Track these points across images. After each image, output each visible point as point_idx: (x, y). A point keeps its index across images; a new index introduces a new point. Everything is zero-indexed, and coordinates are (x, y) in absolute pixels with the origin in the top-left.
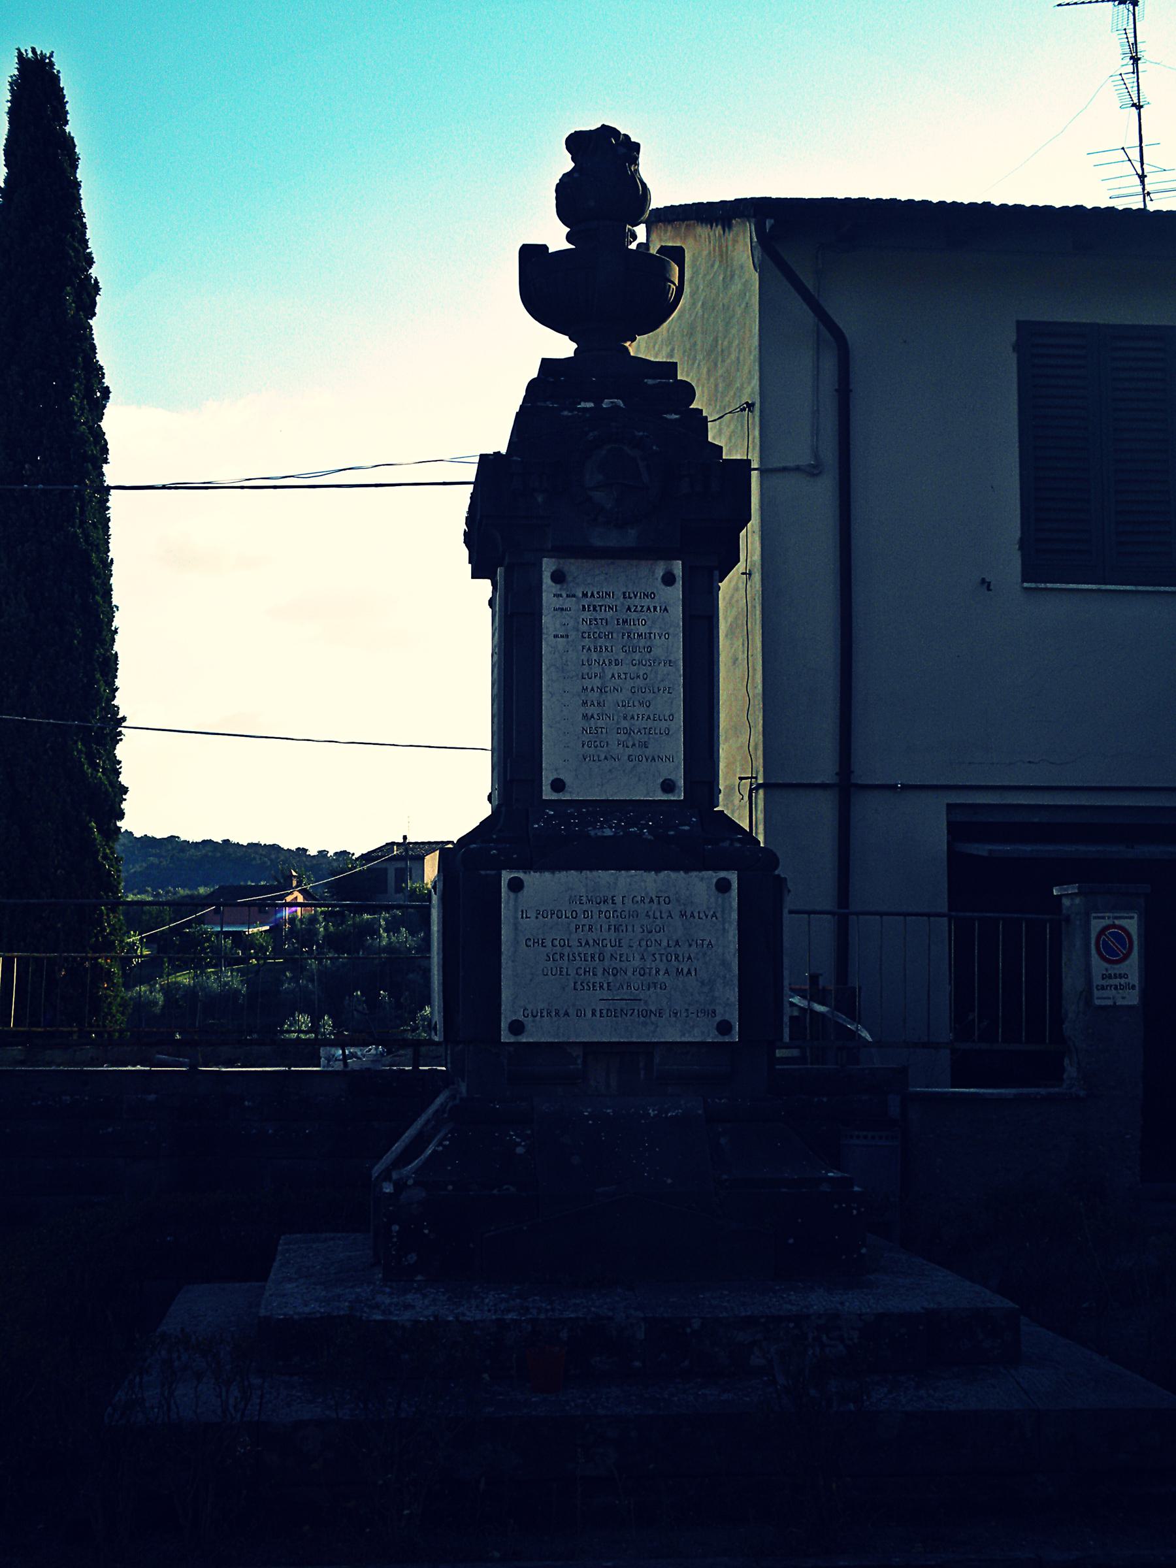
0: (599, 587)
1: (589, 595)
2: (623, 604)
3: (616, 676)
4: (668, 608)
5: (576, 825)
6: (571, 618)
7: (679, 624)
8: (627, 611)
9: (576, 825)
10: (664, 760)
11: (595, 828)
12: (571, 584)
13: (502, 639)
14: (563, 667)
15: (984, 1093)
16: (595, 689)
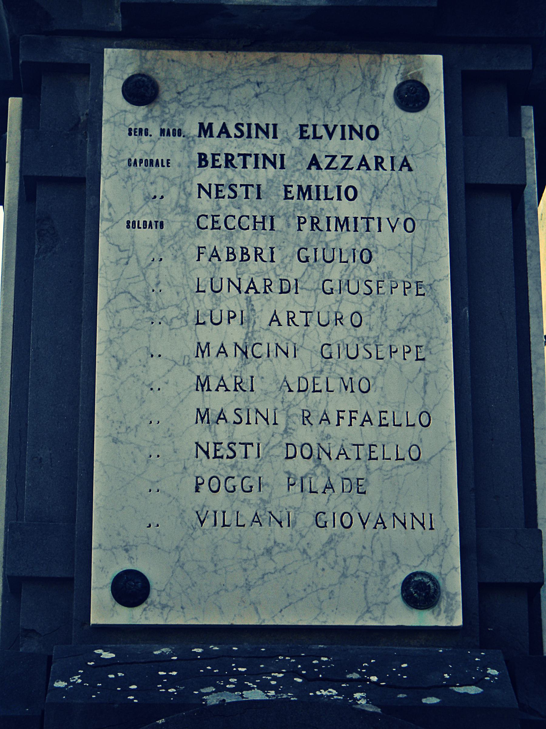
0: (240, 115)
1: (216, 129)
2: (299, 151)
3: (283, 319)
4: (410, 160)
5: (172, 682)
6: (172, 183)
7: (437, 197)
8: (309, 168)
9: (172, 682)
10: (409, 525)
11: (220, 689)
12: (173, 107)
13: (365, 51)
14: (147, 297)
15: (10, 173)
16: (230, 350)
